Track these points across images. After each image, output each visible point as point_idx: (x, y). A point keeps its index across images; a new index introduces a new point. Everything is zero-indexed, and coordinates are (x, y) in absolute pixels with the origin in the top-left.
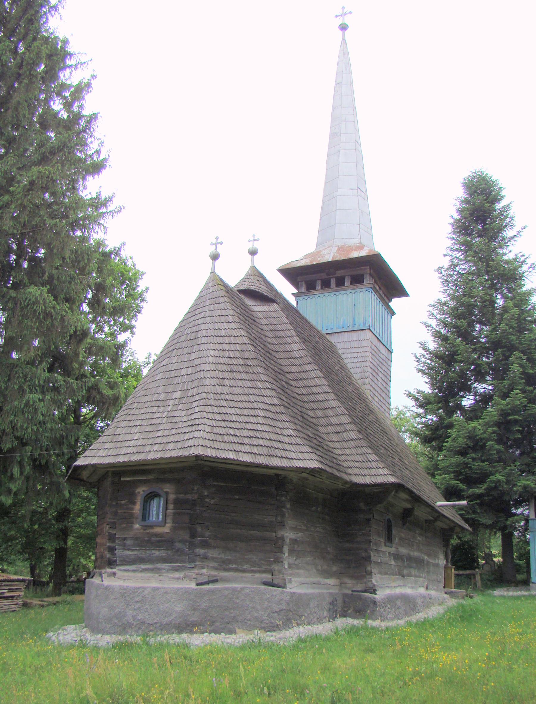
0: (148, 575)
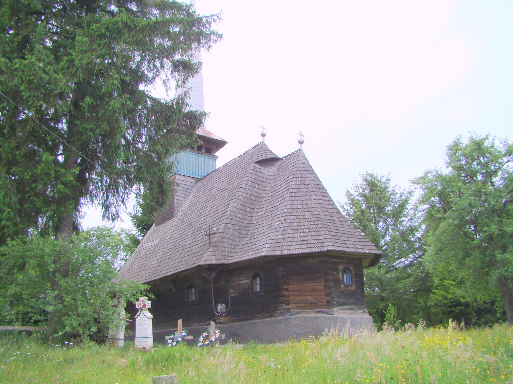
0: (351, 311)
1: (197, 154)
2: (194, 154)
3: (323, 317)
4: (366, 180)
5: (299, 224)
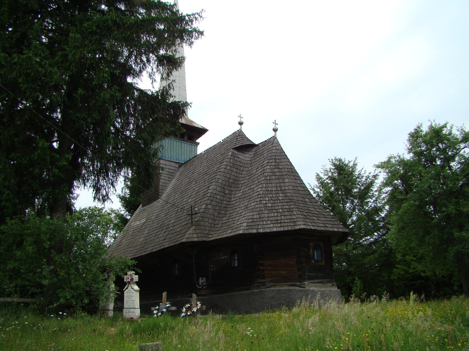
0: (321, 285)
1: (180, 141)
2: (177, 140)
3: (295, 289)
4: (334, 165)
5: (274, 205)
